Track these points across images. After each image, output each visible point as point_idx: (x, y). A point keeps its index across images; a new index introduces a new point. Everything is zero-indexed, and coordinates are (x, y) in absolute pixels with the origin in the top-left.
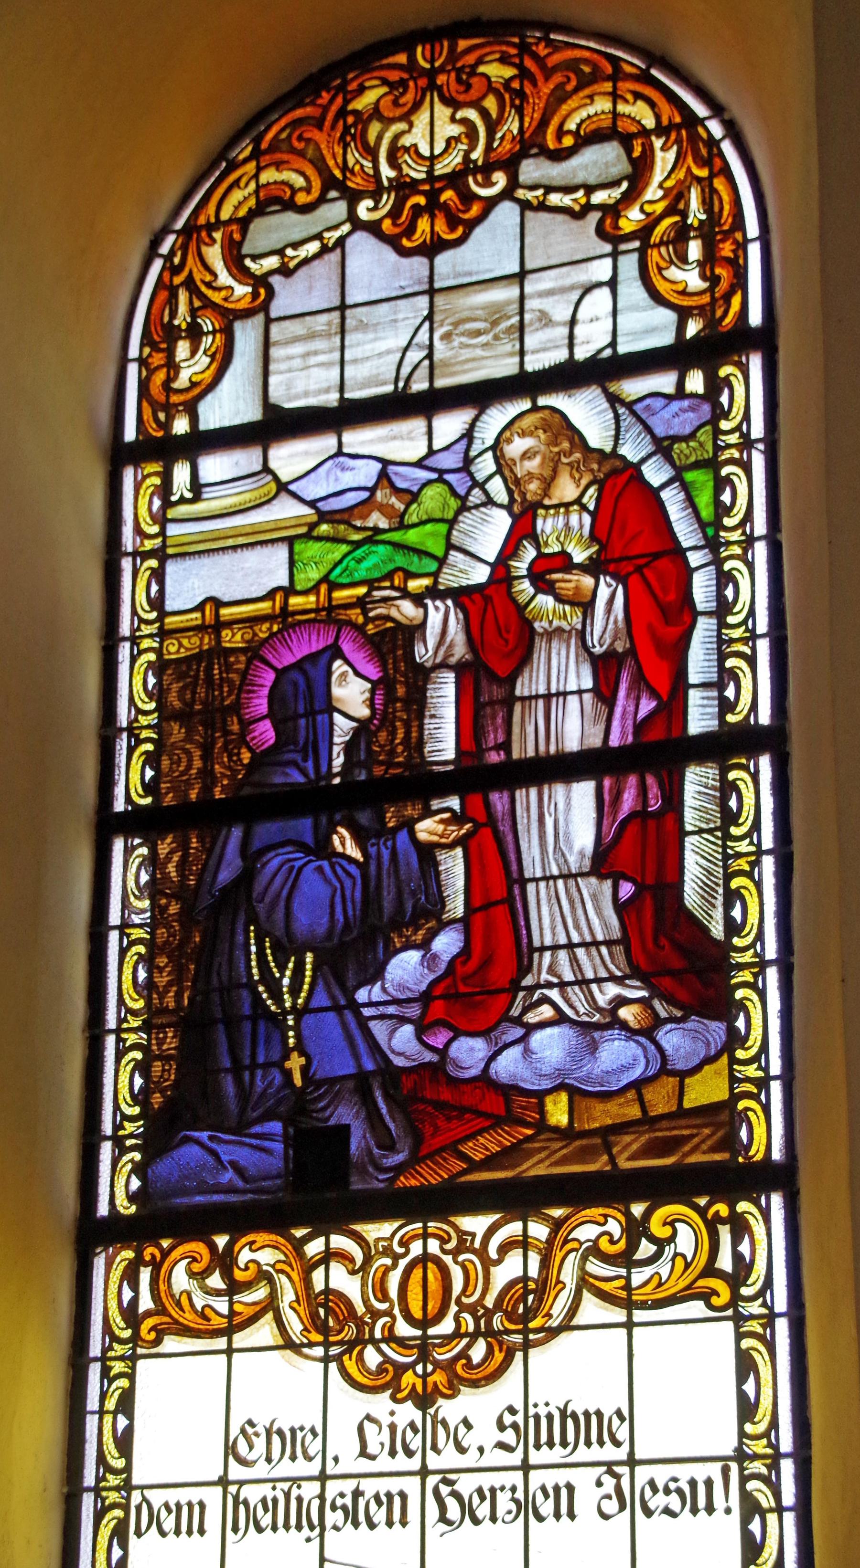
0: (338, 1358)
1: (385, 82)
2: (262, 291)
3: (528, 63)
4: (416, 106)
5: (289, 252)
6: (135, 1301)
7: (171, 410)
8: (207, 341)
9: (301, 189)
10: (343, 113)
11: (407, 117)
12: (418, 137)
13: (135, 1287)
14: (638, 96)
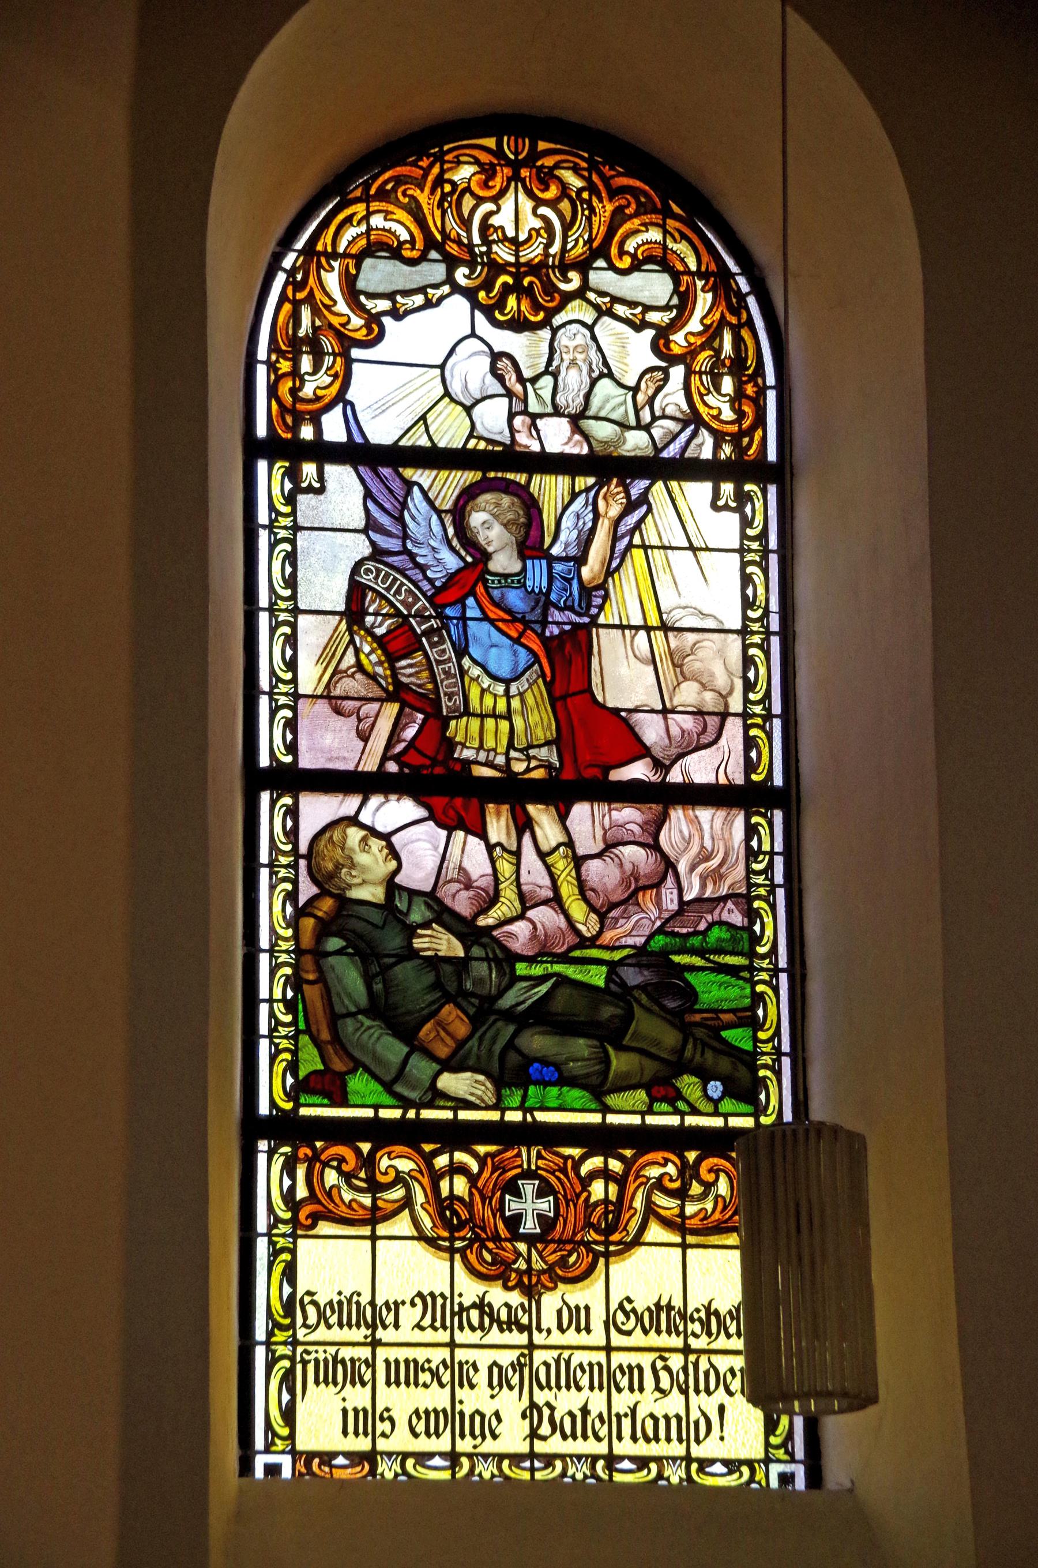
0: (462, 1251)
1: (477, 162)
2: (375, 326)
3: (595, 178)
4: (503, 192)
5: (399, 298)
6: (292, 1188)
7: (299, 420)
8: (328, 361)
9: (406, 242)
10: (439, 181)
11: (495, 199)
12: (504, 219)
13: (293, 1177)
14: (684, 237)
